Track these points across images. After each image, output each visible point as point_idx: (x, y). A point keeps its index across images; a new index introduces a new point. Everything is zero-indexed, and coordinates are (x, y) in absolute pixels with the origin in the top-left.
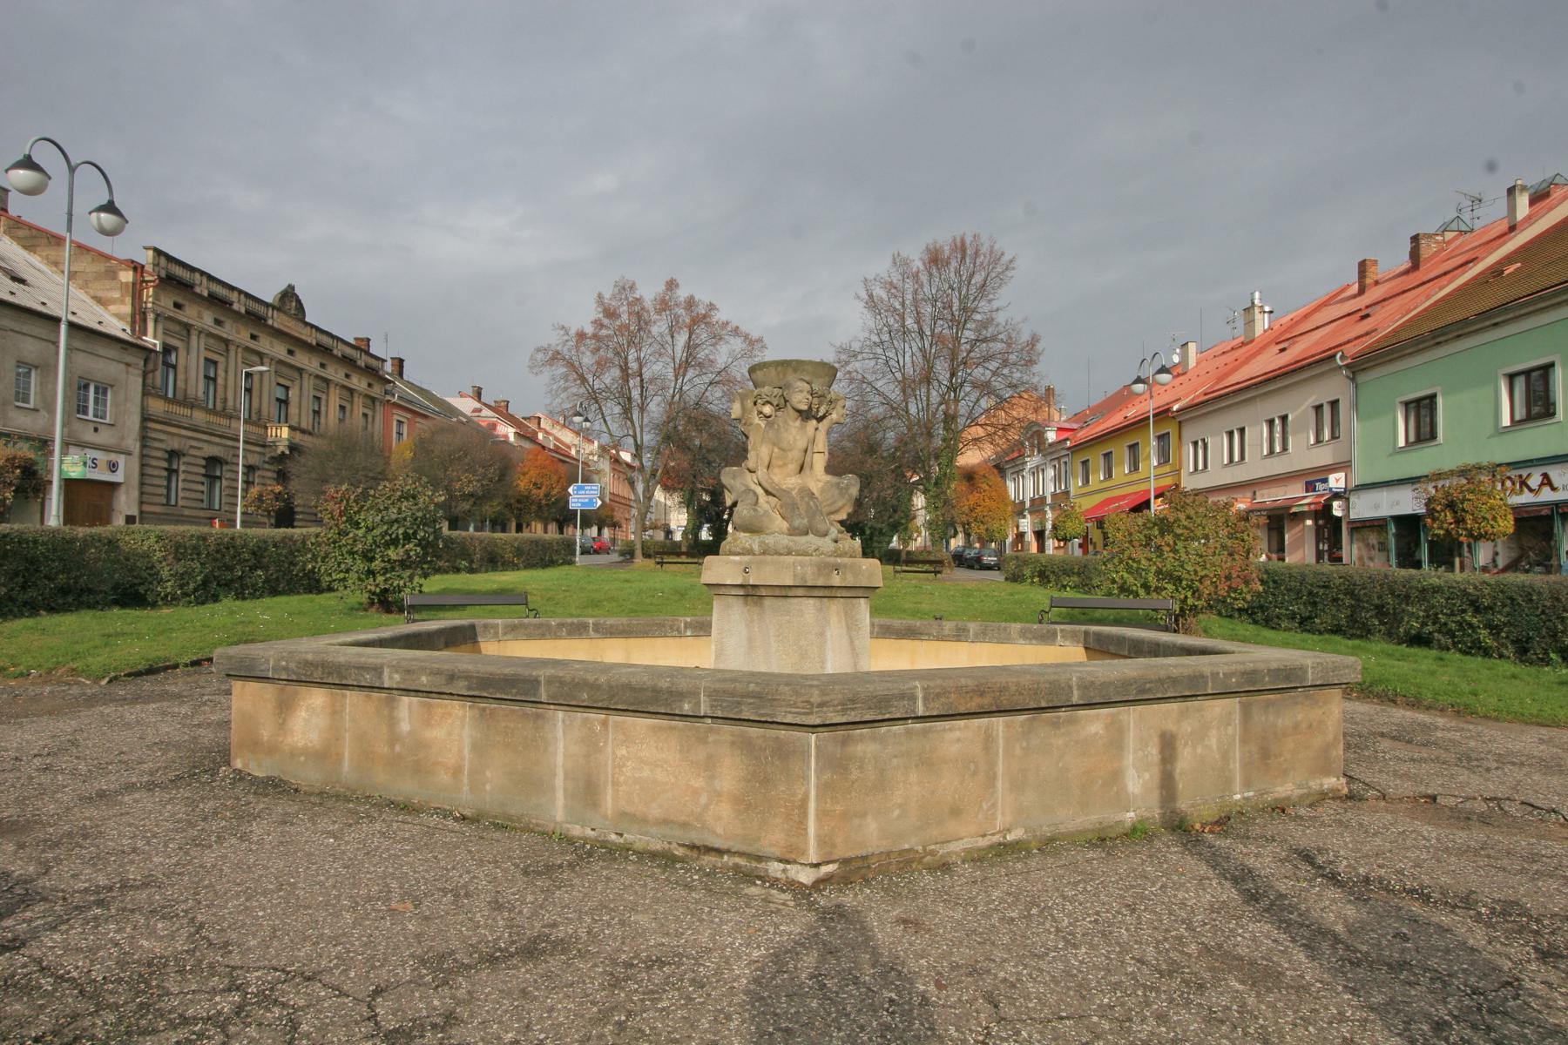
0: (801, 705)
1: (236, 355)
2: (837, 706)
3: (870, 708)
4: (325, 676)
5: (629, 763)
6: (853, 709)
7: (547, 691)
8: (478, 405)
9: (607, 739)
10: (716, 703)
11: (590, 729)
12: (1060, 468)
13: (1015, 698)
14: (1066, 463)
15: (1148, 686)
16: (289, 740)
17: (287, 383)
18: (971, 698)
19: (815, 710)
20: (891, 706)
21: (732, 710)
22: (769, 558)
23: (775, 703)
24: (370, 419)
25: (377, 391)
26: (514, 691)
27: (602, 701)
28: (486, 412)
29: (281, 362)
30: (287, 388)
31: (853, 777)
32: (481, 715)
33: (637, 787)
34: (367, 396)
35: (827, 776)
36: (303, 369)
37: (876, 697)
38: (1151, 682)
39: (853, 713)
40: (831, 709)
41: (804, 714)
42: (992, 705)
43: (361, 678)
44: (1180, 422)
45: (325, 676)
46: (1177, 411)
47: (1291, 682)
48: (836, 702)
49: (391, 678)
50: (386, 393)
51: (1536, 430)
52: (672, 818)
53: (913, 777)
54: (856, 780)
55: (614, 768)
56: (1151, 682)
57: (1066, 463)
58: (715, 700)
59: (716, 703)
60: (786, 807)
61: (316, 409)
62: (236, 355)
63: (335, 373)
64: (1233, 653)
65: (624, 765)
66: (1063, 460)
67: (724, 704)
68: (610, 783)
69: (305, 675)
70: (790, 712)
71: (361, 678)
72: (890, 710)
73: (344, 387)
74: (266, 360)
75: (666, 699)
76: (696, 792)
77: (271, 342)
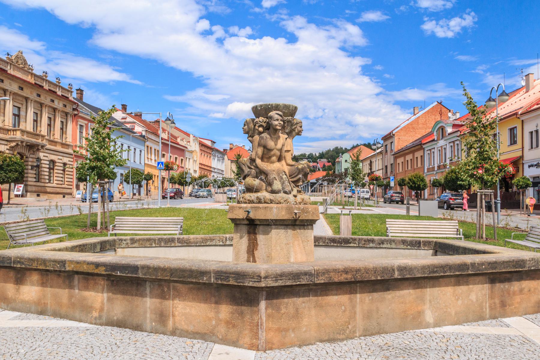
0: (256, 277)
1: (26, 228)
2: (273, 278)
3: (289, 279)
4: (38, 265)
5: (180, 306)
6: (281, 280)
7: (142, 272)
8: (124, 115)
9: (170, 295)
10: (218, 277)
11: (162, 290)
12: (442, 152)
13: (364, 275)
14: (458, 144)
15: (435, 269)
16: (21, 297)
17: (20, 106)
18: (341, 275)
19: (263, 280)
20: (300, 278)
21: (226, 280)
22: (261, 205)
23: (244, 277)
24: (65, 124)
25: (69, 109)
26: (127, 272)
27: (167, 276)
28: (129, 119)
29: (15, 94)
30: (19, 108)
31: (282, 312)
32: (112, 284)
33: (183, 317)
34: (63, 112)
35: (270, 311)
36: (27, 98)
37: (292, 274)
38: (436, 268)
39: (281, 281)
40: (270, 279)
41: (258, 282)
42: (352, 278)
43: (55, 266)
44: (522, 121)
45: (38, 265)
46: (521, 114)
47: (516, 268)
48: (272, 276)
49: (69, 266)
50: (74, 109)
51: (533, 158)
52: (199, 332)
53: (313, 312)
54: (284, 313)
55: (173, 308)
56: (436, 268)
57: (458, 144)
58: (218, 276)
59: (218, 277)
60: (250, 326)
61: (35, 119)
62: (26, 228)
63: (46, 99)
64: (499, 253)
65: (178, 307)
66: (456, 143)
67: (222, 278)
68: (171, 315)
69: (29, 265)
70: (251, 281)
71: (55, 266)
72: (300, 280)
73: (50, 107)
74: (8, 93)
75: (196, 275)
76: (210, 319)
77: (10, 83)
